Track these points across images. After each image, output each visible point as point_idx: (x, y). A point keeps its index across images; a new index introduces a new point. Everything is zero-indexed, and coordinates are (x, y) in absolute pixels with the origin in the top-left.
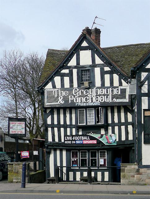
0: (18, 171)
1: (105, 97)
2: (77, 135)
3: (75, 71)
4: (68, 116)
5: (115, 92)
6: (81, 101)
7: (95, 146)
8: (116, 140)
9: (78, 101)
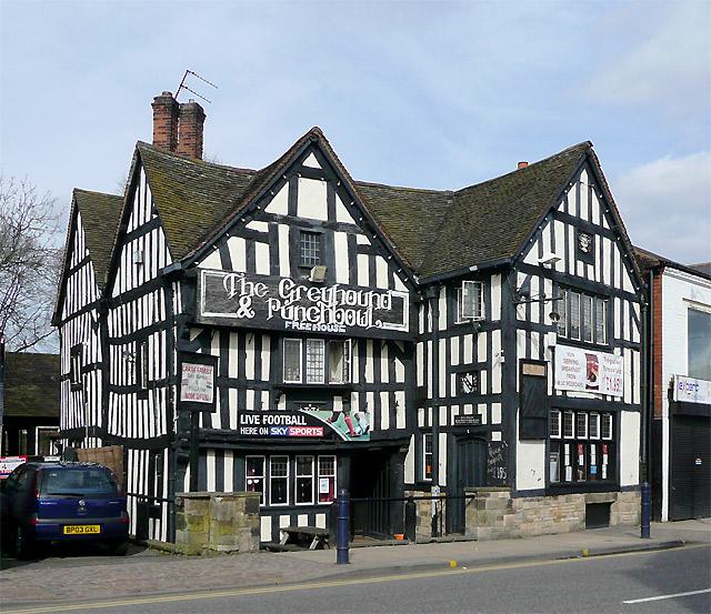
0: (232, 518)
1: (359, 312)
2: (273, 411)
3: (284, 230)
4: (250, 353)
5: (380, 305)
6: (300, 317)
7: (318, 444)
8: (368, 428)
9: (290, 317)
